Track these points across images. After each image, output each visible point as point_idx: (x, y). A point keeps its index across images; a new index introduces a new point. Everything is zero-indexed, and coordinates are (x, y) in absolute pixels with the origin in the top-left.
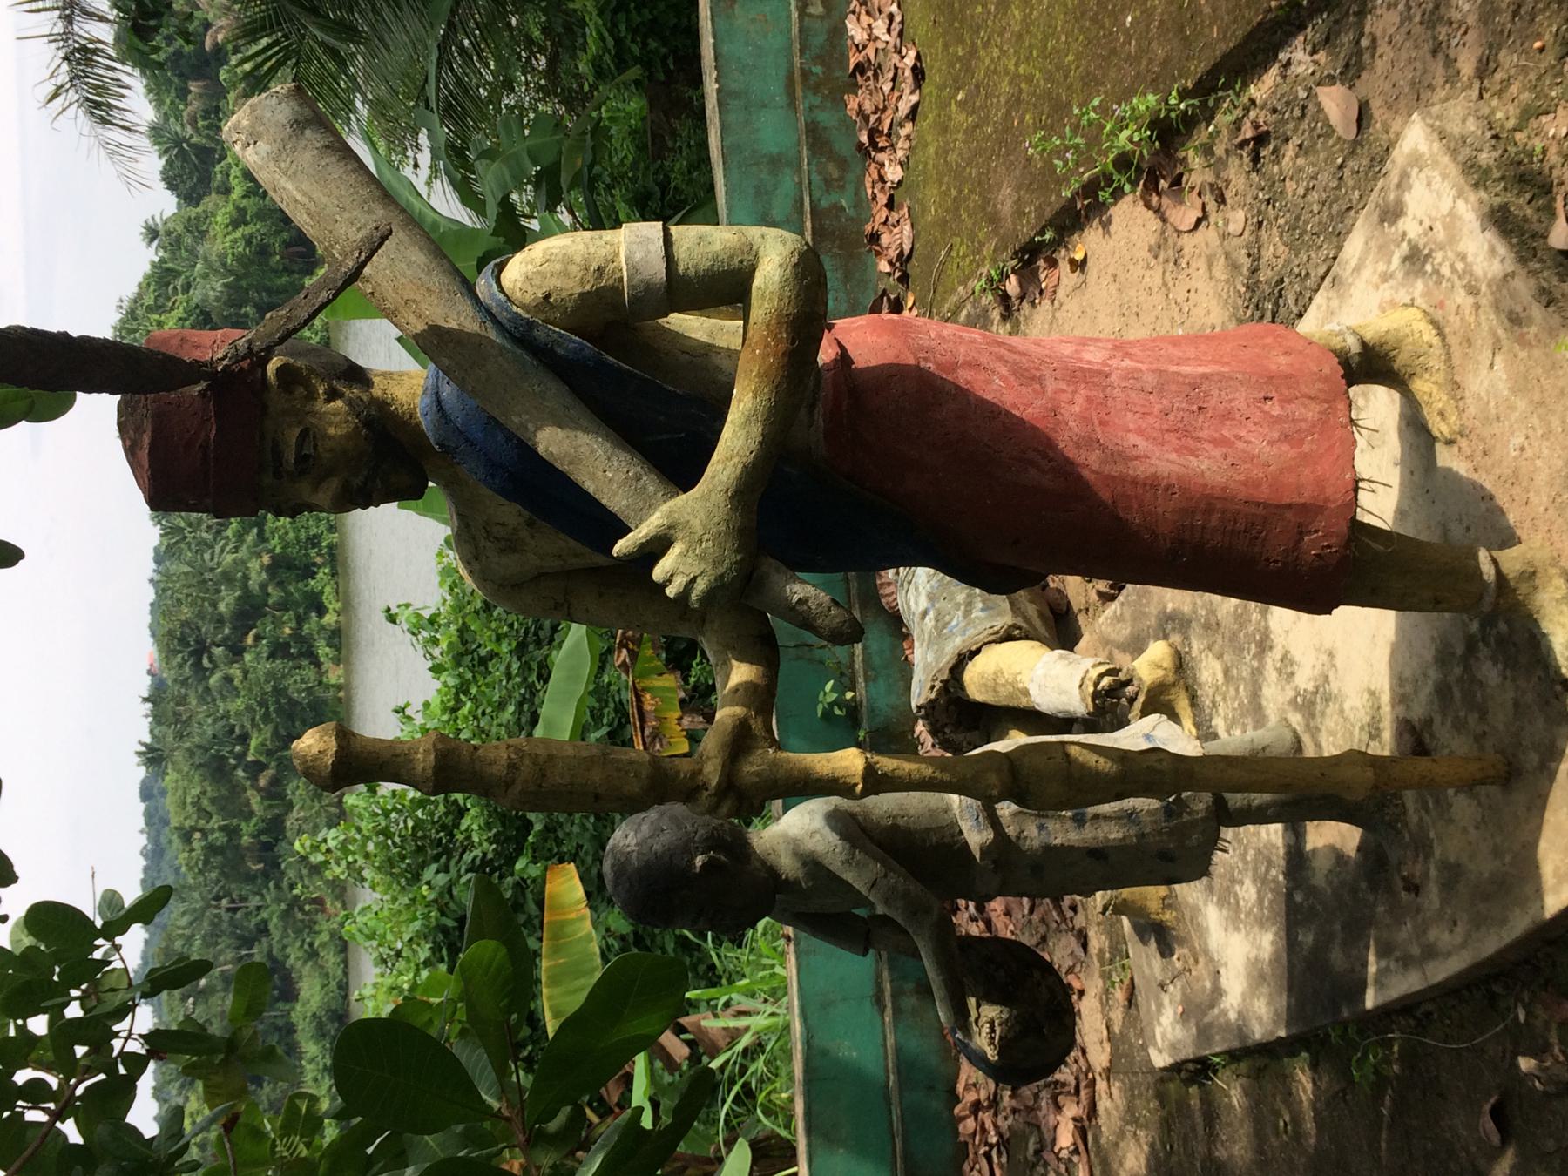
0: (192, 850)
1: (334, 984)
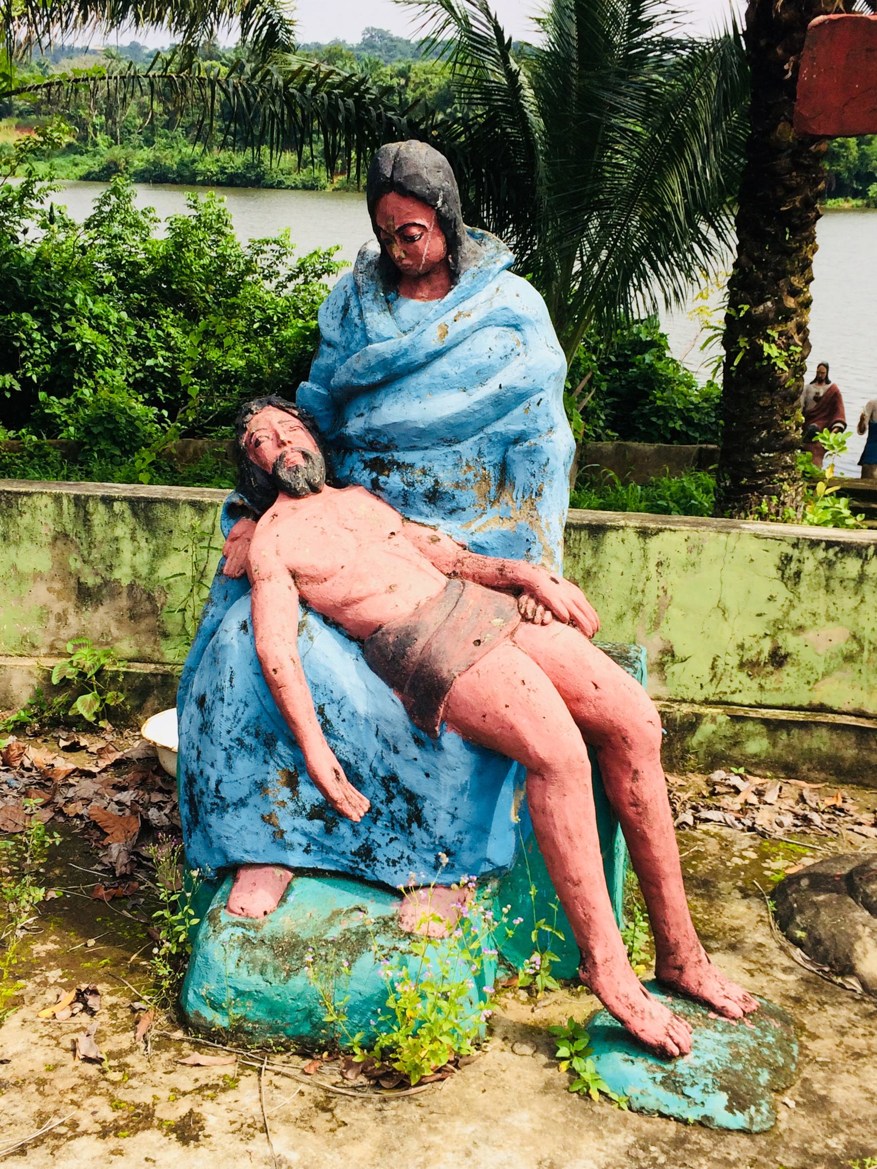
1: (282, 178)
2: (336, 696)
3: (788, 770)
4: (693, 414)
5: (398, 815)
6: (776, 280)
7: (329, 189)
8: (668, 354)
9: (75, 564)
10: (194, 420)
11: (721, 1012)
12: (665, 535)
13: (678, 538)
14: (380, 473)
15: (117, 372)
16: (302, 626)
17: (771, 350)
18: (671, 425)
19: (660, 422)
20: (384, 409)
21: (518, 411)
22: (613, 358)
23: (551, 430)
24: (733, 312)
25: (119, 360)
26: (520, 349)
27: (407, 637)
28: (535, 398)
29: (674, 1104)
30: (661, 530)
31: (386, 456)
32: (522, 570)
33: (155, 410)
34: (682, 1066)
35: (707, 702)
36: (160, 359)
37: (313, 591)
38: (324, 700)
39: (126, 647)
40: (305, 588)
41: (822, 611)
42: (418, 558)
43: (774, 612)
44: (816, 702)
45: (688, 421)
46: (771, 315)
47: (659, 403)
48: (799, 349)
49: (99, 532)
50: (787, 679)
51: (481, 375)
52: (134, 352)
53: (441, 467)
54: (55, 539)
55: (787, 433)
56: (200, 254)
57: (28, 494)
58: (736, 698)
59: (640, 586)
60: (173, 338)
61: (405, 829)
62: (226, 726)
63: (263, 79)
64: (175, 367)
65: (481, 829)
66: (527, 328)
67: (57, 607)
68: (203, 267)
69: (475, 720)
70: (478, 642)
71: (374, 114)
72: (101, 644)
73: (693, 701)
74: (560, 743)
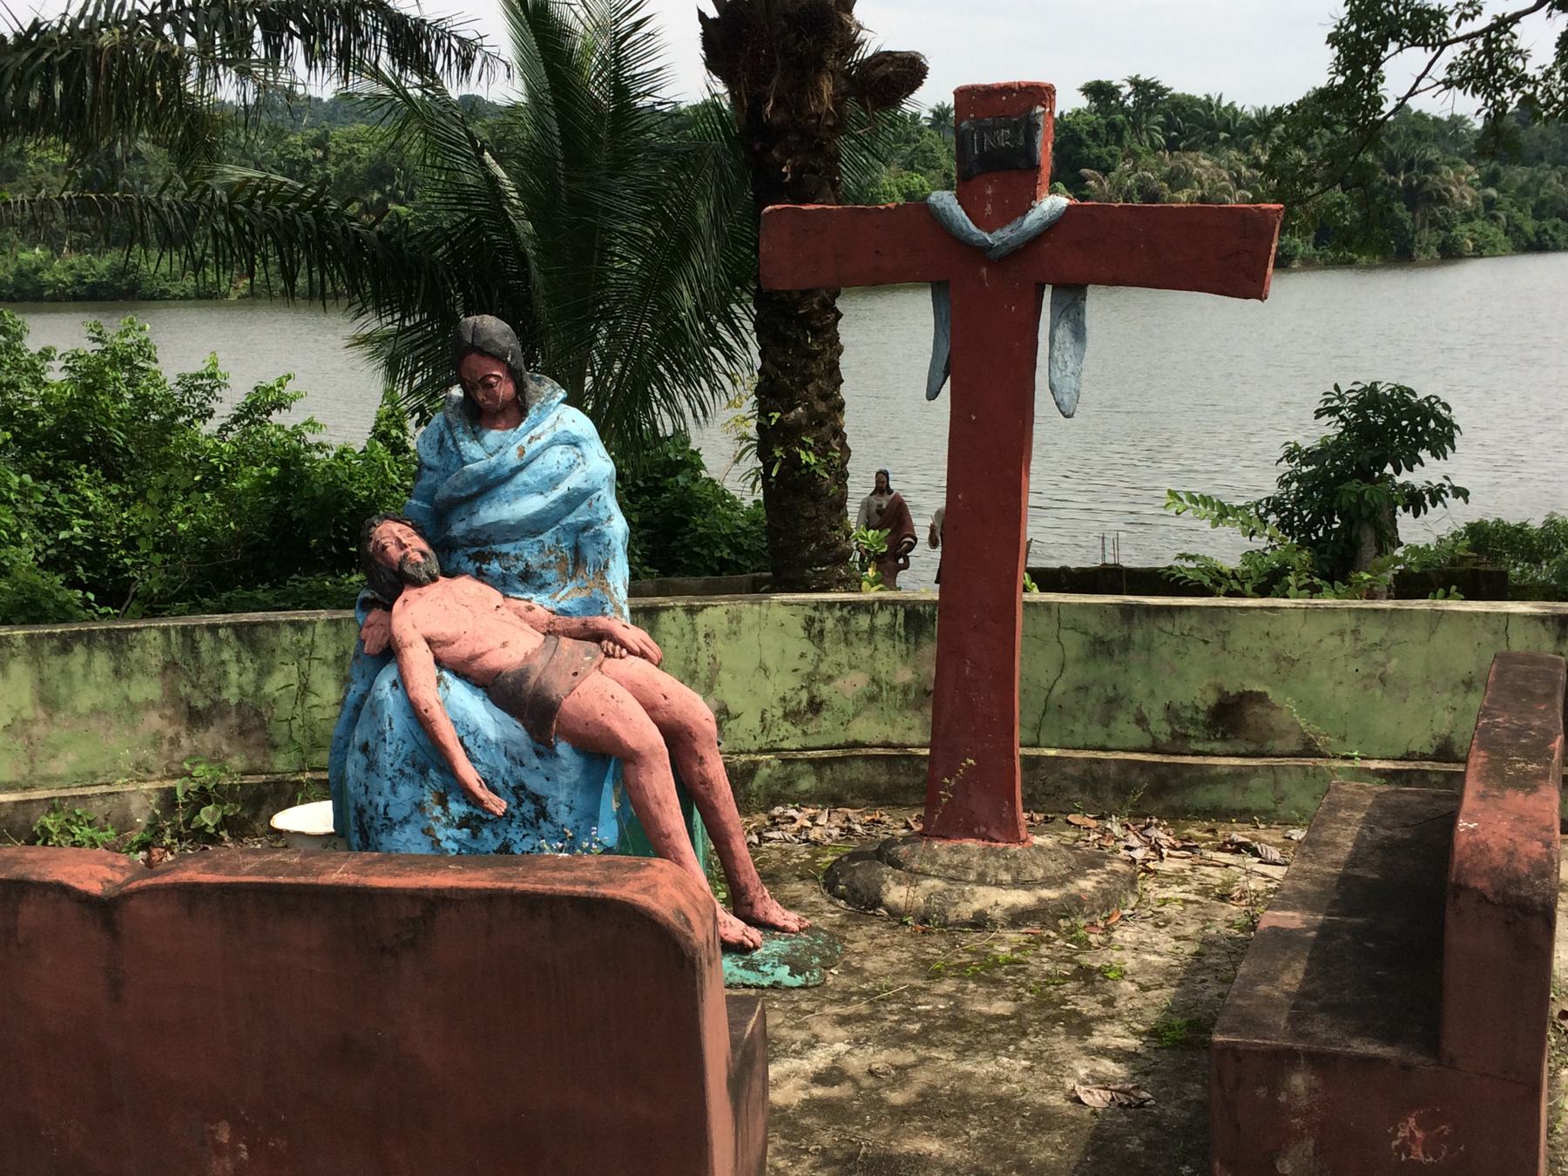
0: (304, 149)
2: (471, 729)
3: (833, 801)
4: (741, 540)
5: (527, 815)
6: (804, 385)
7: (233, 297)
8: (704, 474)
9: (185, 690)
10: (160, 592)
11: (784, 929)
12: (710, 610)
13: (720, 612)
14: (483, 562)
15: (25, 550)
16: (439, 679)
17: (807, 457)
18: (717, 554)
19: (705, 552)
20: (481, 513)
21: (583, 506)
22: (641, 484)
23: (609, 519)
24: (764, 421)
25: (24, 535)
26: (580, 460)
27: (522, 675)
28: (596, 495)
29: (752, 977)
30: (705, 607)
31: (486, 549)
32: (602, 622)
33: (79, 593)
34: (756, 955)
35: (761, 751)
36: (77, 530)
37: (445, 652)
38: (463, 733)
39: (237, 762)
40: (438, 651)
41: (844, 661)
42: (519, 622)
43: (806, 667)
44: (850, 740)
45: (736, 549)
46: (804, 422)
47: (701, 530)
48: (837, 455)
49: (206, 657)
50: (825, 724)
51: (553, 481)
52: (41, 522)
53: (530, 553)
54: (165, 668)
55: (836, 544)
56: (117, 396)
57: (138, 630)
58: (785, 745)
59: (693, 656)
60: (91, 503)
61: (534, 825)
62: (390, 760)
63: (203, 194)
64: (97, 538)
65: (593, 817)
66: (583, 445)
67: (170, 732)
68: (121, 412)
69: (580, 729)
70: (575, 674)
71: (338, 228)
72: (214, 762)
73: (749, 752)
74: (644, 734)
